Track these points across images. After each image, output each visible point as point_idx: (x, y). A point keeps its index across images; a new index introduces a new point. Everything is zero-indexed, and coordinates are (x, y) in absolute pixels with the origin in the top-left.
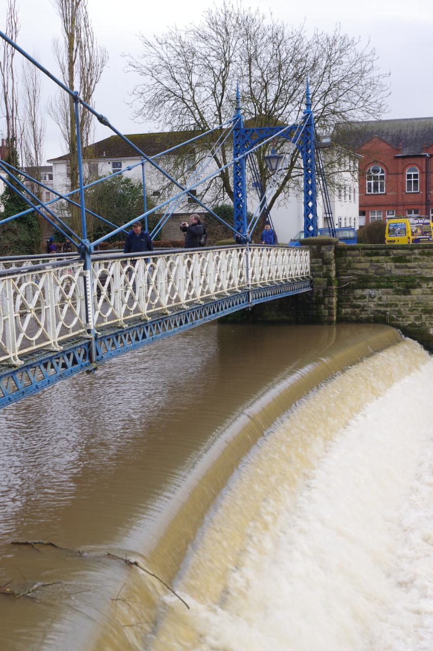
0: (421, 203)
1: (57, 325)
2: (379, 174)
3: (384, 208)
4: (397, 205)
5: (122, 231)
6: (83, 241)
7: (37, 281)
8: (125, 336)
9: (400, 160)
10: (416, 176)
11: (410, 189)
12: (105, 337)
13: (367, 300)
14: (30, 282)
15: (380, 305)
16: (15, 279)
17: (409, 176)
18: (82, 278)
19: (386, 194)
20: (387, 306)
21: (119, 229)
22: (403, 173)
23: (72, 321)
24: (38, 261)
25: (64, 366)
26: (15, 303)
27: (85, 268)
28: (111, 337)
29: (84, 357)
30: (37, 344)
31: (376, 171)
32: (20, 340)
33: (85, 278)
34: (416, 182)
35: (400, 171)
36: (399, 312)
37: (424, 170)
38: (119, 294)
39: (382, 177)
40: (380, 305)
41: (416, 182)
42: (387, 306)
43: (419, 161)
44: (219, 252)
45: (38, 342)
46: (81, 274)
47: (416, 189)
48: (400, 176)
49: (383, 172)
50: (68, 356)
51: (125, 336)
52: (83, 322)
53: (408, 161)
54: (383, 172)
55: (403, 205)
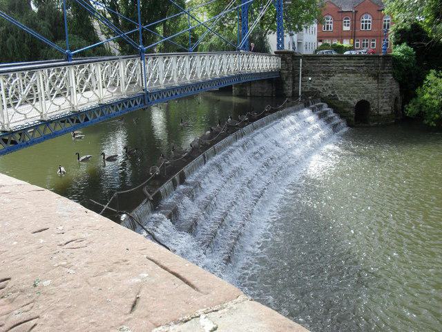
25: (130, 106)
46: (139, 63)
52: (141, 85)
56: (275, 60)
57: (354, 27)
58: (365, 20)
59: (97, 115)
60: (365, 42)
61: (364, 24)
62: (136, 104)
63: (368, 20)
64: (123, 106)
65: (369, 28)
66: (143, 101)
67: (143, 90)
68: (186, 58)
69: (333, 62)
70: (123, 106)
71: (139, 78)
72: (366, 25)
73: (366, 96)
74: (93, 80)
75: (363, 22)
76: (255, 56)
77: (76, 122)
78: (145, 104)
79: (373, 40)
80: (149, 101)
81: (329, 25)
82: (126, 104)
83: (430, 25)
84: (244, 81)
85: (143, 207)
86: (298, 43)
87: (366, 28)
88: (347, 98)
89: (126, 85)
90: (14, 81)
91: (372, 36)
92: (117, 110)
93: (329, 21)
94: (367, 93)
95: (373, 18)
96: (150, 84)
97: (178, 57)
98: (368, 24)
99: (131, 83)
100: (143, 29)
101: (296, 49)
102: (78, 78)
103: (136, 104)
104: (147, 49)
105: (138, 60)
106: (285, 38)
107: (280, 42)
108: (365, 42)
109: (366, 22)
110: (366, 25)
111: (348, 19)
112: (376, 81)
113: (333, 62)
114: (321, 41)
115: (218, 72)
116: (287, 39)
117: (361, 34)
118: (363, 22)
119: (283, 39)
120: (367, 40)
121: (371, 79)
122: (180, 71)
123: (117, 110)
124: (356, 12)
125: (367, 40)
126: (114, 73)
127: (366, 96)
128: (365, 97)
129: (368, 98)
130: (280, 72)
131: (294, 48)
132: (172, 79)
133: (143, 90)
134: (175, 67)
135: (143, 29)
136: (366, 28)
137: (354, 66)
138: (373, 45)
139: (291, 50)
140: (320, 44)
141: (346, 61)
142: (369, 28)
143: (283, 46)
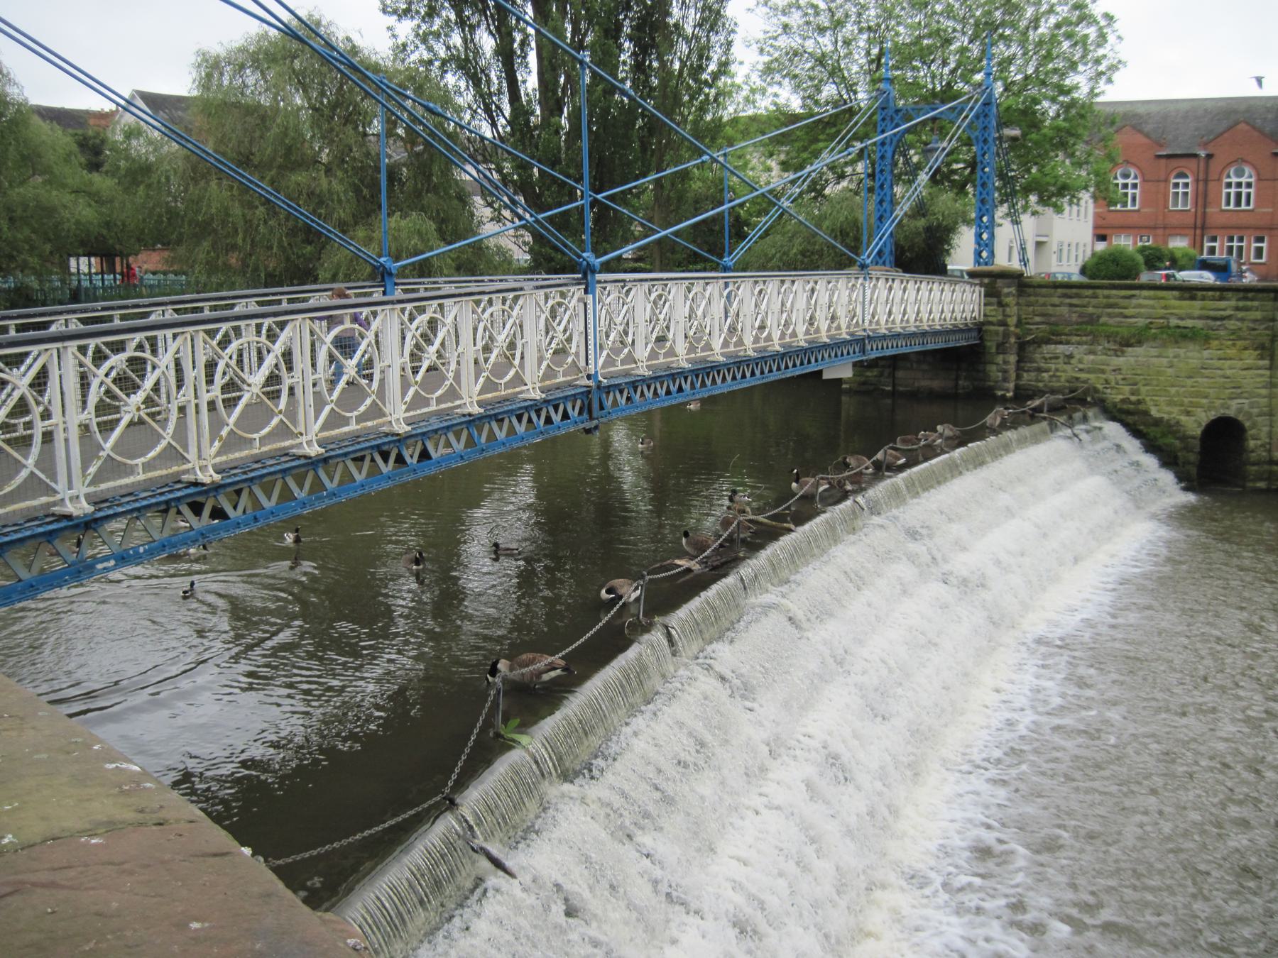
0: (1168, 232)
1: (477, 380)
2: (1130, 181)
3: (1143, 232)
4: (1155, 228)
5: (666, 236)
6: (585, 255)
7: (272, 337)
8: (649, 388)
9: (1163, 161)
10: (1186, 185)
11: (1176, 204)
12: (615, 386)
13: (1060, 360)
14: (249, 336)
15: (1081, 370)
16: (211, 334)
17: (1177, 185)
18: (582, 305)
19: (1138, 211)
20: (1089, 371)
21: (663, 233)
22: (1167, 181)
23: (507, 374)
24: (112, 316)
25: (549, 420)
26: (403, 344)
27: (586, 292)
28: (366, 453)
29: (580, 413)
30: (358, 422)
31: (1126, 176)
32: (481, 380)
33: (585, 305)
34: (1186, 194)
35: (1163, 177)
36: (1107, 381)
37: (1201, 176)
38: (681, 325)
39: (1135, 186)
40: (1081, 370)
41: (1186, 194)
42: (1089, 371)
43: (1192, 163)
44: (793, 282)
45: (507, 385)
46: (580, 300)
47: (1185, 204)
48: (1162, 185)
49: (1136, 177)
50: (556, 408)
51: (649, 388)
52: (582, 364)
53: (1174, 163)
54: (1136, 177)
55: (1165, 228)
56: (968, 295)
57: (1203, 198)
58: (1234, 180)
59: (659, 390)
60: (1235, 244)
61: (1233, 190)
62: (566, 416)
63: (1244, 180)
64: (530, 420)
65: (1248, 203)
66: (587, 409)
67: (589, 377)
68: (714, 289)
69: (1140, 306)
70: (530, 420)
71: (577, 339)
72: (1239, 195)
73: (1234, 404)
74: (450, 344)
75: (1229, 185)
76: (923, 286)
77: (396, 461)
78: (591, 418)
79: (1260, 240)
80: (602, 408)
81: (1244, 190)
82: (556, 411)
83: (1086, 188)
84: (873, 355)
85: (1062, 419)
86: (1039, 245)
87: (1238, 203)
88: (1175, 410)
89: (646, 344)
90: (234, 345)
91: (1257, 228)
92: (375, 471)
93: (1128, 182)
94: (1238, 396)
95: (1258, 174)
96: (609, 362)
97: (783, 282)
98: (1130, 191)
99: (556, 352)
100: (595, 203)
101: (1031, 263)
102: (409, 336)
103: (566, 416)
104: (602, 264)
105: (578, 291)
106: (997, 231)
107: (985, 246)
108: (1235, 244)
109: (1239, 185)
110: (1239, 195)
111: (1185, 176)
112: (1266, 362)
113: (1140, 306)
114: (1102, 238)
115: (801, 329)
116: (1004, 234)
117: (1221, 220)
118: (1229, 185)
119: (992, 236)
120: (1241, 239)
121: (1250, 357)
122: (785, 315)
123: (375, 471)
124: (1209, 156)
125: (1241, 239)
126: (622, 315)
127: (1234, 404)
128: (1232, 409)
129: (1240, 411)
130: (980, 330)
131: (1024, 261)
132: (770, 334)
133: (589, 377)
134: (682, 311)
135: (595, 203)
136: (1238, 203)
137: (1200, 318)
138: (1259, 252)
139: (1016, 265)
140: (1101, 246)
141: (1177, 303)
142: (1248, 203)
143: (992, 254)
